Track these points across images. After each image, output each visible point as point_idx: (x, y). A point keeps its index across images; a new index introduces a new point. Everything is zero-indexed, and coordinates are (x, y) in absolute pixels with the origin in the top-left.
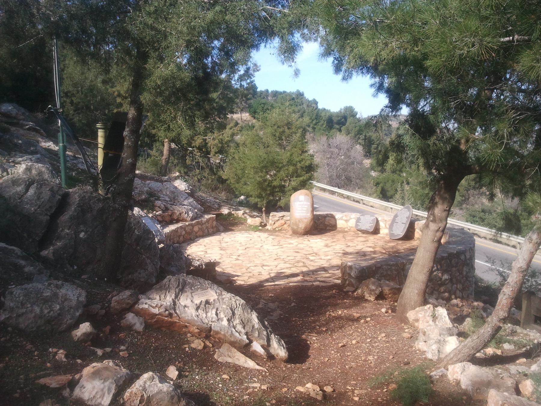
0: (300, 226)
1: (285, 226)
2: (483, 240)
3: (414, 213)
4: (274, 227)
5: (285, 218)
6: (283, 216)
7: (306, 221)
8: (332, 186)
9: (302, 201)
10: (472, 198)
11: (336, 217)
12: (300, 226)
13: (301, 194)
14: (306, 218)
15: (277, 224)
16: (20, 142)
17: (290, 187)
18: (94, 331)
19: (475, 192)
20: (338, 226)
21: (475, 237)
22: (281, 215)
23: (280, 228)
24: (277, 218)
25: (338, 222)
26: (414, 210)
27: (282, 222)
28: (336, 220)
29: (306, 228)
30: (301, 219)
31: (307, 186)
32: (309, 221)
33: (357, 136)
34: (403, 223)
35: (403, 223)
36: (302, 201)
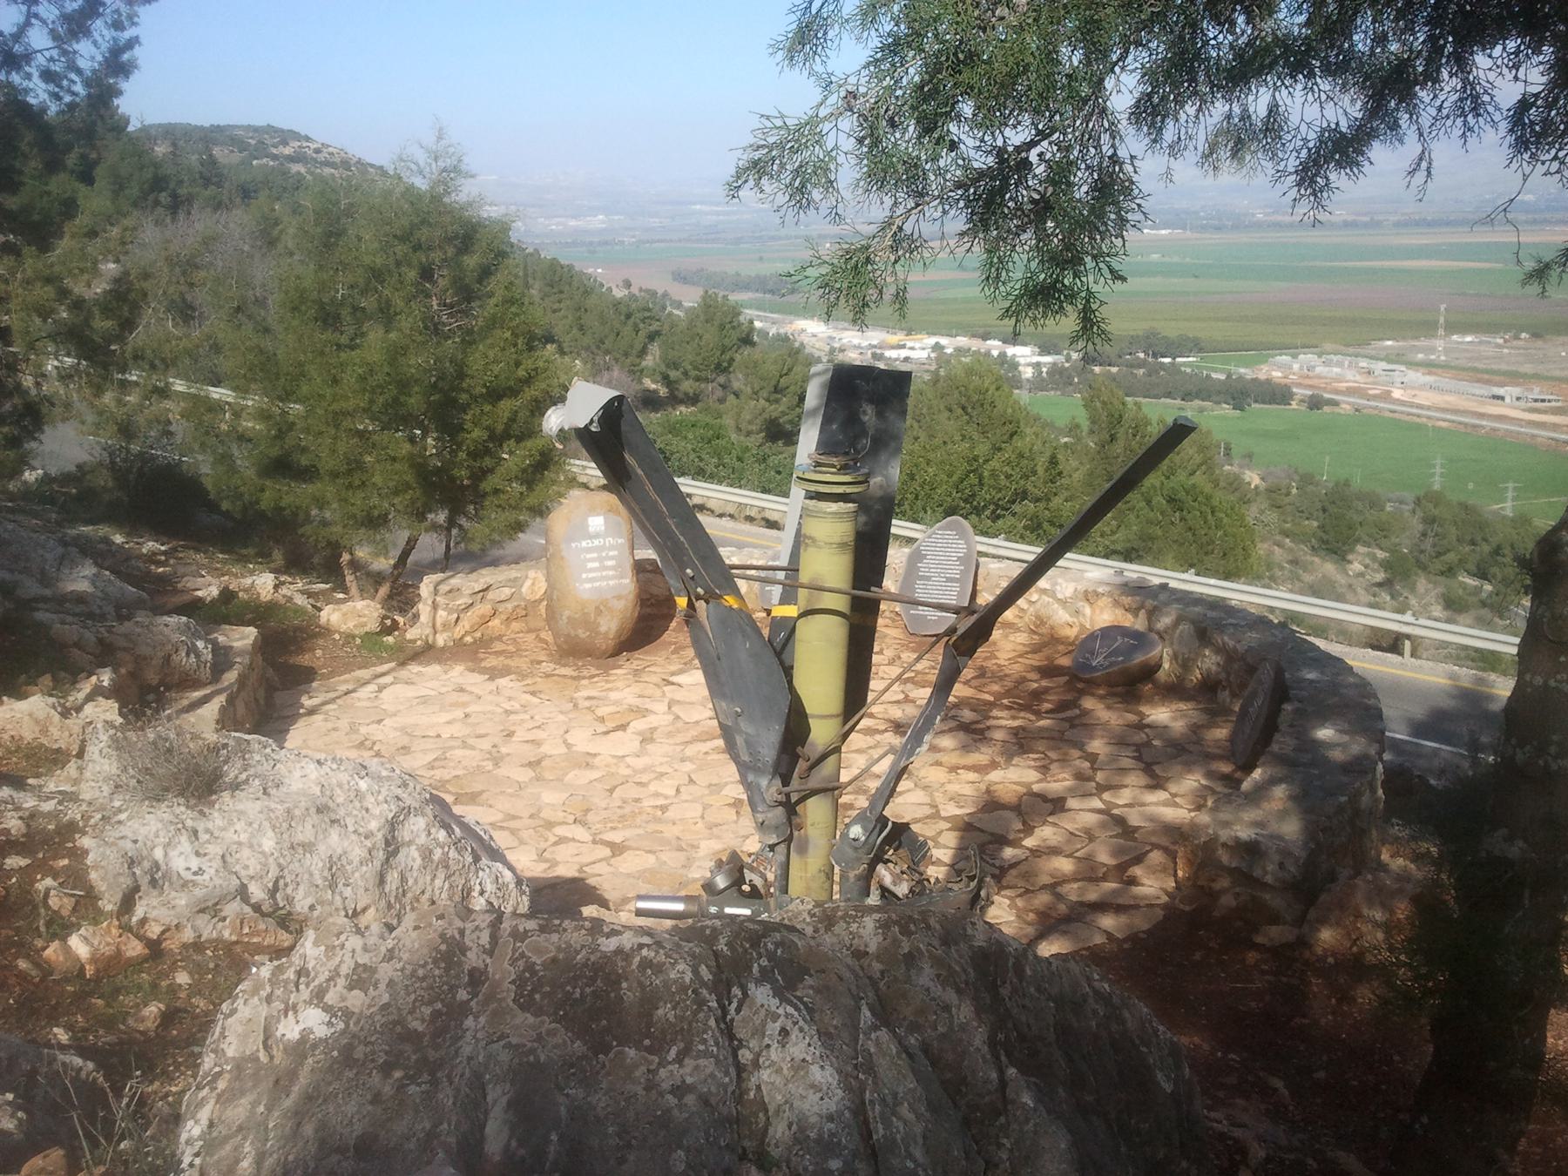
0: (603, 629)
1: (496, 622)
2: (725, 521)
4: (458, 631)
5: (490, 595)
7: (620, 605)
8: (765, 491)
9: (597, 536)
12: (603, 629)
14: (619, 598)
15: (465, 624)
16: (554, 1137)
21: (700, 517)
23: (478, 635)
24: (462, 601)
26: (978, 538)
27: (484, 609)
29: (619, 633)
32: (630, 605)
33: (151, 198)
34: (949, 580)
35: (949, 580)
36: (597, 536)
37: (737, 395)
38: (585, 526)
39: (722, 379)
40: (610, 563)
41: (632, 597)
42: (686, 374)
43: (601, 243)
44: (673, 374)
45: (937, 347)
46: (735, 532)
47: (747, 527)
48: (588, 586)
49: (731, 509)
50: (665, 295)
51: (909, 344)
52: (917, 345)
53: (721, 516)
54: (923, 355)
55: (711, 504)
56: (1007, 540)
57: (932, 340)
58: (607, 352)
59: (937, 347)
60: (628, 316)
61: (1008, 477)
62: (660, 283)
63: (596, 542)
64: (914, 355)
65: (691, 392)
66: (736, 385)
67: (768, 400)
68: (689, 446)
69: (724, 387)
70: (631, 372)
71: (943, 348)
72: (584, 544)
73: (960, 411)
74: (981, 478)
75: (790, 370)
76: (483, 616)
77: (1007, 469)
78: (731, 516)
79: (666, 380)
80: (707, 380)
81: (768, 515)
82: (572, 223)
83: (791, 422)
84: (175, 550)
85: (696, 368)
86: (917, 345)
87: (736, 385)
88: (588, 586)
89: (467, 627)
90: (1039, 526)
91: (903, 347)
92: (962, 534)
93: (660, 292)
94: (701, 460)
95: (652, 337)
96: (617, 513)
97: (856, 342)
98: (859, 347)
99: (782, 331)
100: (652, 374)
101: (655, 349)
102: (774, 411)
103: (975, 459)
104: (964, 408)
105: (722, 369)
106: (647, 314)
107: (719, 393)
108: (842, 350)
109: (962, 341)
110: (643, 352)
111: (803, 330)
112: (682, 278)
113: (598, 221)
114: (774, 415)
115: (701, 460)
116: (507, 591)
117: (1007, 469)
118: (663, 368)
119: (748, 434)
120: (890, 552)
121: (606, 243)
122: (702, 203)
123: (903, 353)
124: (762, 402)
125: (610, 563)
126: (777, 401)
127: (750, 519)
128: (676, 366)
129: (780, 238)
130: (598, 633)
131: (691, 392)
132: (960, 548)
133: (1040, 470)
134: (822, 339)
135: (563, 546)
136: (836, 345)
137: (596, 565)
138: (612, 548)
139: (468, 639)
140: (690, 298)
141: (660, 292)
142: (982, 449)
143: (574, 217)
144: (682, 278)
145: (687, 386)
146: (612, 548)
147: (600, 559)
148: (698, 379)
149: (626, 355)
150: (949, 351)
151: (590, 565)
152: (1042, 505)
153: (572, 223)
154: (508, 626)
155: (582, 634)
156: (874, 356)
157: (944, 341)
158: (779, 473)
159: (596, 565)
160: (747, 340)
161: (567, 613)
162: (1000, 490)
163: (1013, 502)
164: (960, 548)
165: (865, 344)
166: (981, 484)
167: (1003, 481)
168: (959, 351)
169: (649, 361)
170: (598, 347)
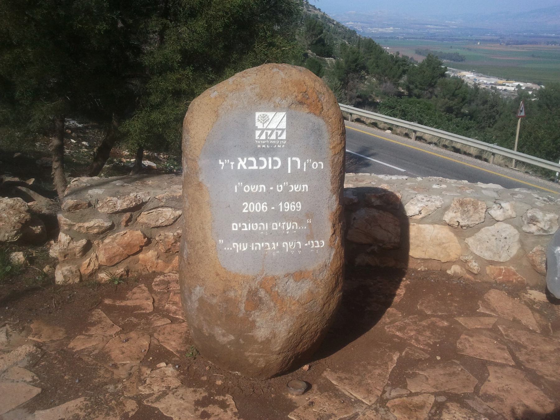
0: (261, 333)
1: (149, 255)
3: (341, 108)
4: (87, 265)
5: (144, 218)
6: (139, 207)
7: (299, 291)
9: (270, 150)
10: (351, 82)
11: (411, 209)
12: (261, 333)
13: (266, 99)
14: (299, 276)
17: (168, 50)
18: (4, 182)
19: (355, 76)
20: (415, 252)
22: (121, 204)
23: (120, 270)
24: (95, 223)
25: (413, 230)
27: (134, 235)
28: (403, 222)
30: (268, 284)
31: (258, 47)
32: (322, 292)
36: (270, 150)
37: (436, 96)
38: (248, 129)
39: (431, 90)
40: (289, 207)
41: (326, 275)
42: (416, 87)
43: (390, 38)
44: (411, 86)
45: (518, 86)
47: (443, 150)
48: (241, 247)
49: (435, 140)
50: (412, 58)
51: (507, 84)
52: (510, 85)
53: (430, 143)
54: (513, 89)
55: (426, 137)
57: (517, 84)
58: (386, 76)
59: (518, 86)
60: (397, 62)
62: (409, 54)
63: (267, 163)
64: (508, 88)
65: (418, 93)
66: (436, 93)
67: (449, 99)
68: (417, 110)
69: (431, 93)
70: (395, 84)
71: (521, 87)
72: (242, 163)
73: (546, 107)
75: (460, 87)
76: (128, 245)
78: (436, 144)
79: (408, 89)
80: (424, 90)
82: (380, 30)
84: (87, 128)
85: (421, 84)
86: (510, 85)
87: (436, 93)
88: (241, 247)
89: (103, 258)
91: (504, 85)
93: (410, 57)
94: (422, 116)
95: (404, 72)
96: (316, 108)
97: (485, 81)
98: (486, 84)
99: (456, 75)
100: (402, 86)
101: (405, 77)
104: (548, 105)
105: (432, 85)
106: (404, 63)
107: (429, 95)
108: (479, 84)
109: (529, 85)
110: (400, 77)
111: (464, 76)
112: (419, 52)
113: (390, 30)
114: (451, 105)
115: (422, 116)
116: (168, 214)
118: (407, 83)
120: (285, 125)
121: (392, 38)
122: (431, 25)
123: (504, 88)
124: (447, 100)
125: (289, 207)
126: (453, 100)
127: (445, 147)
128: (412, 83)
129: (460, 40)
130: (252, 340)
131: (418, 93)
134: (471, 80)
135: (202, 163)
136: (477, 82)
137: (263, 207)
138: (297, 177)
139: (103, 276)
140: (420, 59)
141: (410, 57)
143: (382, 28)
144: (419, 52)
145: (416, 91)
146: (297, 177)
147: (271, 198)
148: (421, 89)
149: (394, 77)
150: (523, 88)
151: (249, 207)
153: (380, 30)
154: (168, 261)
155: (223, 336)
156: (492, 88)
157: (521, 84)
158: (458, 126)
159: (263, 207)
160: (443, 75)
161: (198, 291)
165: (489, 83)
168: (528, 89)
169: (402, 81)
170: (383, 74)
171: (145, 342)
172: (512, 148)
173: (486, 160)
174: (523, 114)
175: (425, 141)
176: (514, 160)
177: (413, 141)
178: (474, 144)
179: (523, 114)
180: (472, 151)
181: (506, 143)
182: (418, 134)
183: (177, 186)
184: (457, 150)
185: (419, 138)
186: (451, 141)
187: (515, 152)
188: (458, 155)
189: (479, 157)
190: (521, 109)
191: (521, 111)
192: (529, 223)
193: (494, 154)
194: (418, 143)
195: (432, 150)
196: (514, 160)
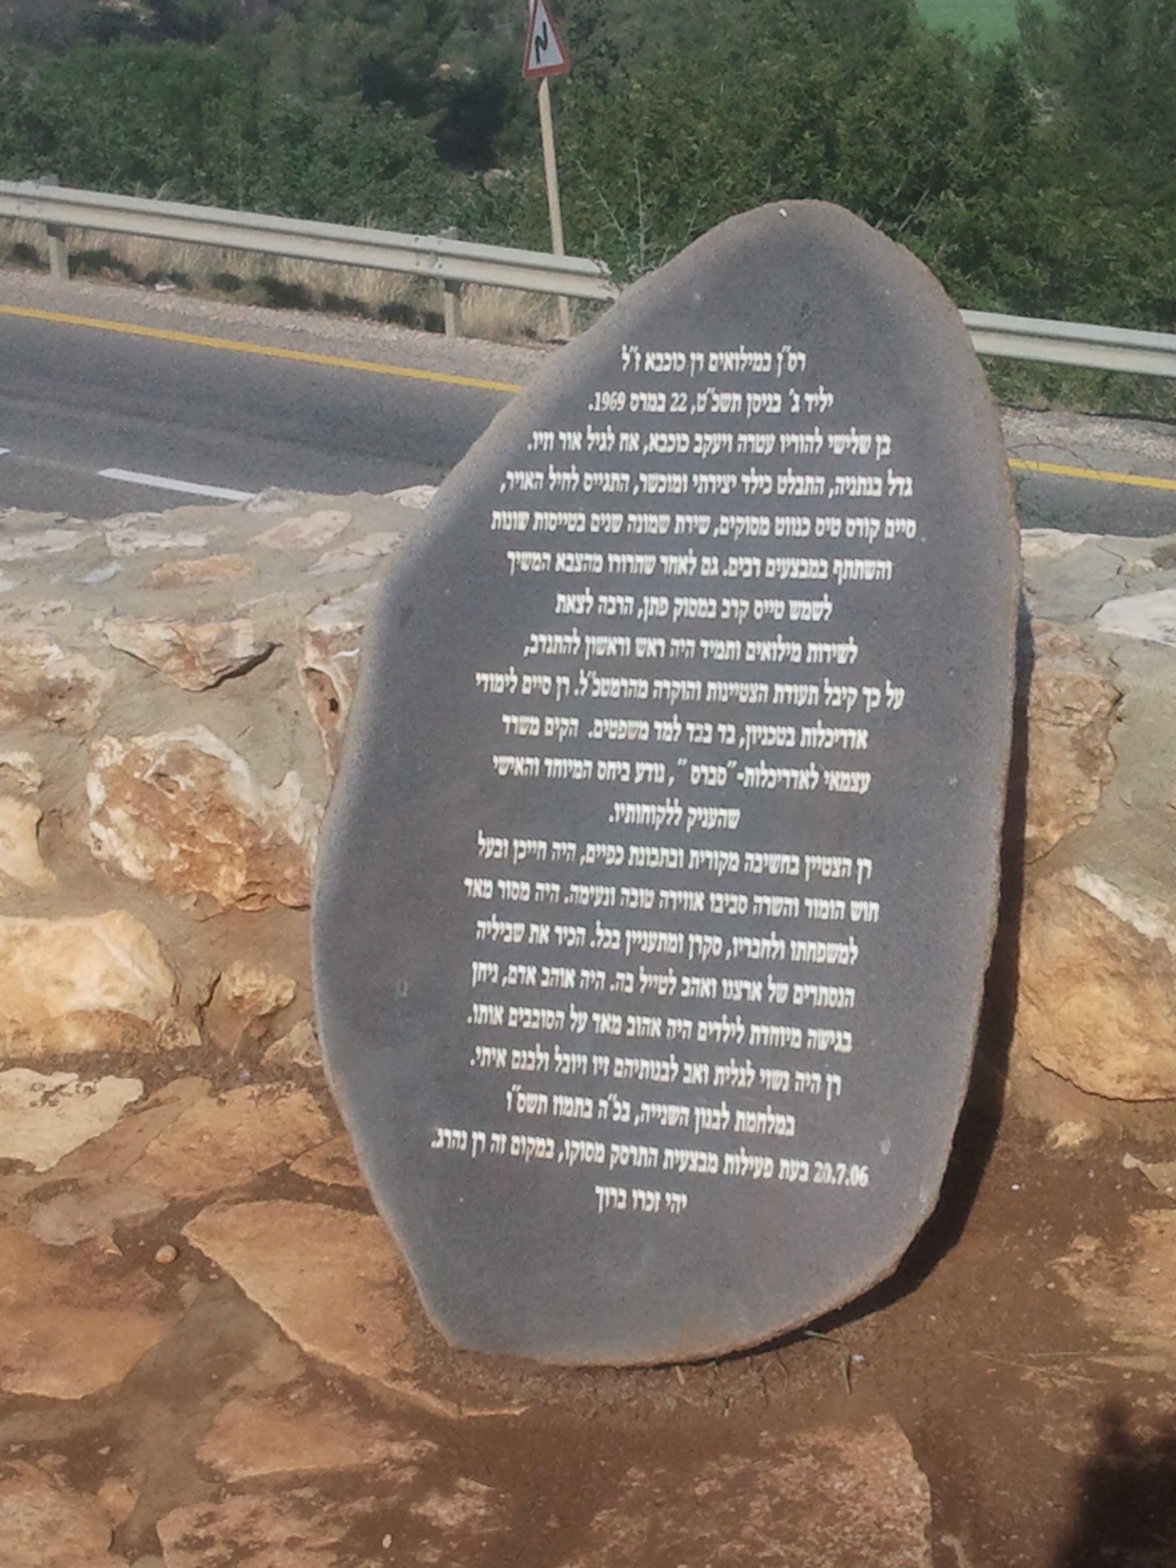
2: (164, 298)
8: (309, 211)
26: (970, 317)
34: (773, 819)
35: (773, 819)
46: (179, 322)
53: (151, 280)
55: (135, 252)
56: (182, 197)
61: (898, 135)
67: (363, 19)
68: (106, 108)
74: (830, 140)
77: (895, 114)
81: (286, 274)
83: (415, 64)
90: (982, 253)
92: (870, 372)
102: (375, 40)
103: (814, 91)
115: (140, 139)
117: (895, 114)
119: (328, 95)
124: (349, 22)
126: (383, 20)
127: (227, 285)
132: (857, 500)
133: (976, 111)
142: (826, 69)
152: (985, 201)
158: (341, 162)
162: (879, 170)
163: (915, 198)
164: (857, 500)
166: (832, 158)
167: (886, 150)
171: (262, 982)
172: (549, 249)
173: (434, 324)
174: (553, 56)
175: (129, 273)
176: (563, 301)
177: (56, 280)
178: (370, 253)
179: (553, 56)
180: (367, 289)
181: (507, 220)
182: (76, 243)
183: (1117, 428)
184: (285, 296)
185: (90, 263)
186: (266, 253)
187: (558, 259)
188: (290, 319)
189: (397, 313)
190: (538, 32)
191: (542, 43)
192: (91, 685)
193: (453, 285)
194: (85, 287)
195: (153, 317)
196: (563, 301)
